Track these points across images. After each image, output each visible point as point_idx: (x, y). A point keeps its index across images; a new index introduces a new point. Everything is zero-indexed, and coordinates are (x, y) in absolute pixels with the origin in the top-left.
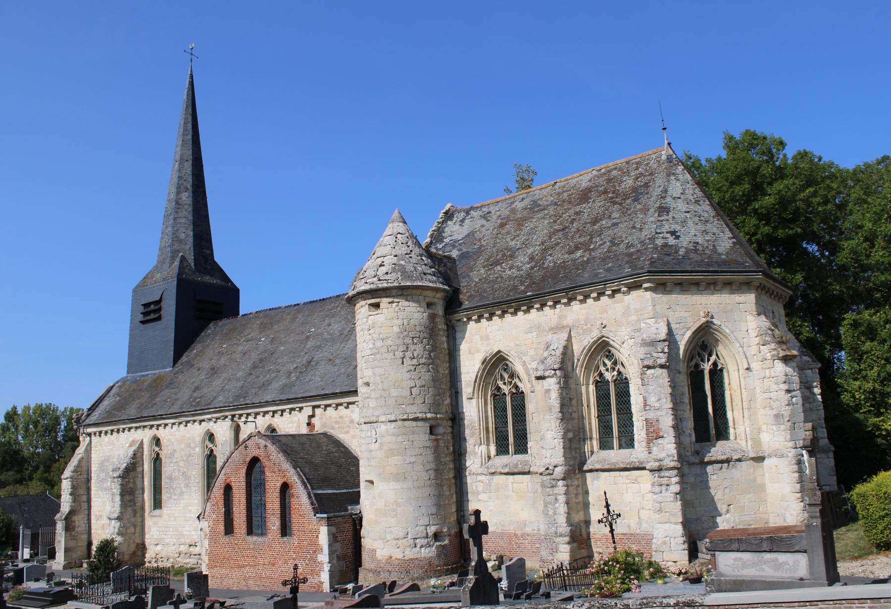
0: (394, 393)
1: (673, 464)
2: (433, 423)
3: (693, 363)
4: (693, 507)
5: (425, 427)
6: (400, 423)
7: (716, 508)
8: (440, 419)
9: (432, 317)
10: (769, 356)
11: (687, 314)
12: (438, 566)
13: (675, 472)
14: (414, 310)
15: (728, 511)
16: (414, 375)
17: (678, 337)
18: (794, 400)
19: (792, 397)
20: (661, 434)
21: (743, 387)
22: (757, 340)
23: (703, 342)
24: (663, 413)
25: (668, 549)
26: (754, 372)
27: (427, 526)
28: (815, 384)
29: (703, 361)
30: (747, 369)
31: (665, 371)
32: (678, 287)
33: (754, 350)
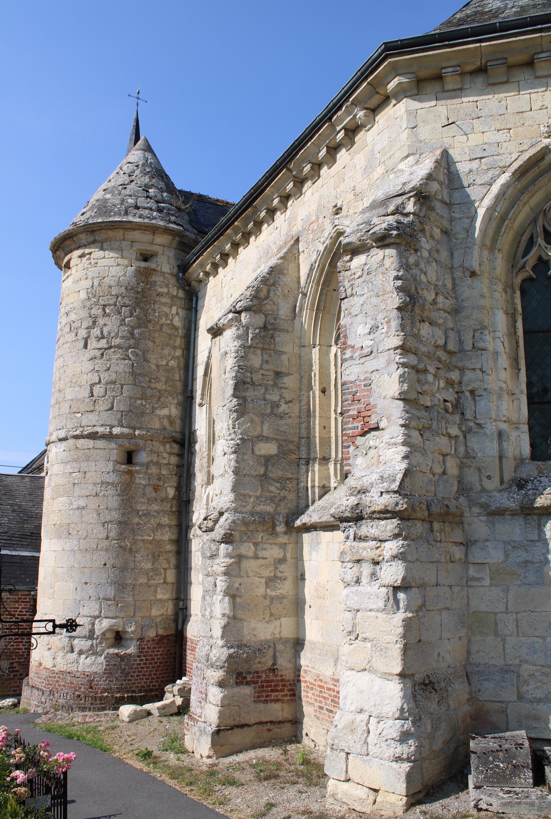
0: (70, 394)
1: (387, 501)
2: (127, 444)
5: (112, 450)
6: (71, 442)
8: (141, 437)
9: (144, 275)
11: (501, 137)
12: (105, 690)
14: (111, 262)
16: (100, 364)
17: (474, 193)
20: (373, 421)
24: (379, 362)
25: (357, 748)
27: (96, 617)
32: (480, 80)
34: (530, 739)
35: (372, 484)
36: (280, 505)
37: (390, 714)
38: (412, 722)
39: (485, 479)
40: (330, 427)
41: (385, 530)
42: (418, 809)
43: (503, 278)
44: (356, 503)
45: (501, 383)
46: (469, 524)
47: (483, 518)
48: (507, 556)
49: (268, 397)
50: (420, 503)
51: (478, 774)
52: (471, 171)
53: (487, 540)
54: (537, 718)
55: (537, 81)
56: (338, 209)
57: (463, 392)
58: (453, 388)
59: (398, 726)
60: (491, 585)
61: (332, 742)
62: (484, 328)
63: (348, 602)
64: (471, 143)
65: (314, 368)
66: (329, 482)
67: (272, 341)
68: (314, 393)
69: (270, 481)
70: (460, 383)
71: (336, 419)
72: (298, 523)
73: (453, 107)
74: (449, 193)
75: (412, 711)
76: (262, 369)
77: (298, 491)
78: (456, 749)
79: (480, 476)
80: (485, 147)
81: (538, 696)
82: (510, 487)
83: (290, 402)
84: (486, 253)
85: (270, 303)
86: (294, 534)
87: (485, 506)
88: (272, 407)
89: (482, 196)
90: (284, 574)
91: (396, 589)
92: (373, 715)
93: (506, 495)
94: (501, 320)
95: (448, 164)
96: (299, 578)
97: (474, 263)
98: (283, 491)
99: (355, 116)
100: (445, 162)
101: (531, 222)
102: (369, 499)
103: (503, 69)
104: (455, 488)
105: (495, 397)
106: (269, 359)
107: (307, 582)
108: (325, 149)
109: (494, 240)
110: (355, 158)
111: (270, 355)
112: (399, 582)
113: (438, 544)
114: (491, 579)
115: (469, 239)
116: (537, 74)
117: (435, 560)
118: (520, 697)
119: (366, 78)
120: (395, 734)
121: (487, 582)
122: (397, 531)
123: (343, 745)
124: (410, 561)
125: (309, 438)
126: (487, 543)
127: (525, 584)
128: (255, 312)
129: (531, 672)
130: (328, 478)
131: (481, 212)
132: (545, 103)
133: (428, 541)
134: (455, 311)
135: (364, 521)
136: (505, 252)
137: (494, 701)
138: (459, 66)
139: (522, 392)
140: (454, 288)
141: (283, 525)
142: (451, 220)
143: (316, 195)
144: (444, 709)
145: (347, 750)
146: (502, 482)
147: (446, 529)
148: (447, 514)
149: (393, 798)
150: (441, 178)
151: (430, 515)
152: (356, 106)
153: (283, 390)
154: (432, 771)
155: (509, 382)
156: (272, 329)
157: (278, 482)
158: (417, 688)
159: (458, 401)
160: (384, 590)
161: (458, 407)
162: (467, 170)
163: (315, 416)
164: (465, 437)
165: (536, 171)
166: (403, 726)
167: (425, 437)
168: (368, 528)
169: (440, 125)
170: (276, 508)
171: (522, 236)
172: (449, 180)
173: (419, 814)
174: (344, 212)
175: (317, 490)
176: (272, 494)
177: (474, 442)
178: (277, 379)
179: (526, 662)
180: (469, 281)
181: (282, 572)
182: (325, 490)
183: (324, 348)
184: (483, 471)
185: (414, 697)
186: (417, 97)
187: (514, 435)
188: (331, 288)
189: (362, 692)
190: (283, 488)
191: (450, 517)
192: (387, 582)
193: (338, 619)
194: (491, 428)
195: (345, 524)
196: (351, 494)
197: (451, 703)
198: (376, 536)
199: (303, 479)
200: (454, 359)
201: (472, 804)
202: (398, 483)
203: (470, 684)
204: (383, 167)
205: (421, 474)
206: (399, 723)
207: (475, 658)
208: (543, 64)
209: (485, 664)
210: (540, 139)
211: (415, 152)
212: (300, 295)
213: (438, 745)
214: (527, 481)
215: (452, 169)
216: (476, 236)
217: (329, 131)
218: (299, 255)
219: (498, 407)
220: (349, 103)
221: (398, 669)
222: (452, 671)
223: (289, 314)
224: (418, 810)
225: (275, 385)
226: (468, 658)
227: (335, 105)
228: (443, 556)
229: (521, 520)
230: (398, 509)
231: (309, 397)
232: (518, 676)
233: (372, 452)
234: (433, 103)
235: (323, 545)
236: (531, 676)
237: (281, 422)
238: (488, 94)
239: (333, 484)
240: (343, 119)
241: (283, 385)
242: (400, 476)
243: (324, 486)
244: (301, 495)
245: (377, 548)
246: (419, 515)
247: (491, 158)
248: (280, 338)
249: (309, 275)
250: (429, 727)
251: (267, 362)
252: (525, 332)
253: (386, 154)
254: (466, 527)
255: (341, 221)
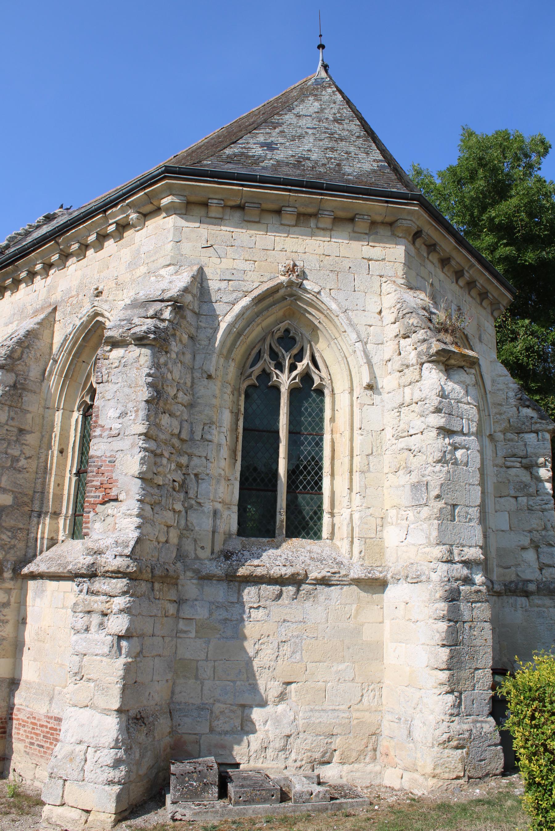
3: (257, 369)
4: (197, 678)
7: (254, 688)
10: (412, 357)
11: (247, 266)
13: (121, 584)
15: (282, 697)
17: (219, 308)
18: (459, 454)
19: (456, 449)
20: (113, 493)
21: (356, 425)
22: (395, 329)
23: (287, 331)
24: (124, 444)
25: (75, 775)
26: (385, 396)
28: (541, 460)
29: (280, 367)
30: (370, 387)
31: (146, 351)
32: (237, 215)
33: (389, 349)
34: (219, 765)
35: (107, 547)
36: (9, 553)
37: (107, 744)
38: (125, 750)
39: (199, 549)
40: (63, 485)
41: (115, 588)
42: (124, 824)
43: (232, 383)
44: (92, 562)
45: (221, 470)
46: (183, 586)
47: (195, 581)
48: (211, 614)
49: (9, 451)
50: (147, 566)
51: (176, 792)
52: (219, 289)
53: (196, 600)
54: (223, 747)
55: (282, 227)
56: (99, 293)
57: (189, 474)
58: (181, 470)
59: (112, 754)
60: (196, 637)
61: (51, 771)
62: (212, 423)
63: (77, 648)
64: (223, 266)
65: (55, 430)
66: (58, 535)
67: (20, 400)
68: (52, 452)
69: (3, 530)
70: (187, 466)
71: (70, 478)
72: (25, 570)
73: (213, 232)
74: (199, 305)
75: (126, 741)
76: (7, 425)
77: (27, 541)
78: (157, 774)
79: (195, 545)
80: (234, 271)
81: (226, 729)
82: (219, 557)
83: (30, 458)
84: (222, 360)
85: (23, 364)
86: (20, 581)
87: (197, 572)
88: (12, 461)
89: (225, 312)
90: (7, 617)
91: (120, 638)
92: (91, 745)
93: (215, 563)
94: (227, 417)
95: (202, 279)
96: (21, 621)
97: (212, 368)
98: (14, 540)
99: (128, 216)
100: (200, 278)
101: (261, 340)
102: (104, 560)
103: (257, 212)
104: (174, 555)
105: (214, 481)
106: (15, 416)
107: (28, 626)
108: (95, 235)
109: (230, 351)
110: (122, 251)
111: (16, 413)
112: (124, 632)
113: (157, 601)
114: (196, 632)
115: (210, 347)
116: (283, 222)
117: (153, 614)
118: (212, 730)
119: (144, 188)
120: (110, 762)
121: (193, 635)
122: (125, 589)
123: (62, 773)
124: (133, 615)
125: (43, 493)
126: (196, 603)
127: (223, 638)
128: (8, 371)
129: (222, 710)
130: (57, 531)
131: (223, 326)
132: (285, 247)
133: (149, 599)
134: (191, 406)
135: (97, 578)
136: (237, 361)
137: (190, 734)
138: (223, 200)
139: (236, 479)
140: (192, 386)
141: (11, 572)
142: (198, 328)
143: (79, 273)
144: (150, 740)
145: (64, 778)
146: (212, 553)
147: (165, 589)
148: (167, 576)
149: (103, 817)
150: (195, 291)
151: (153, 576)
152: (130, 208)
153: (24, 446)
154: (137, 792)
155: (227, 469)
156: (21, 389)
157: (10, 531)
158: (130, 722)
159: (184, 481)
160: (110, 638)
161: (183, 487)
162: (217, 288)
163: (51, 474)
164: (186, 512)
165: (271, 300)
166: (117, 754)
167: (155, 511)
168: (100, 585)
169: (200, 245)
170: (6, 555)
171: (252, 349)
172: (201, 293)
173: (125, 828)
174: (104, 297)
175: (45, 542)
176: (3, 542)
177: (193, 517)
178: (20, 436)
179: (219, 701)
180: (205, 382)
181: (5, 616)
182: (53, 542)
183: (67, 412)
184: (198, 542)
185: (128, 729)
186: (185, 216)
187: (226, 513)
188: (81, 360)
189: (82, 725)
190: (14, 537)
191: (169, 579)
192: (113, 632)
193: (56, 662)
194: (208, 507)
195: (80, 579)
196: (88, 554)
197: (156, 735)
198: (107, 592)
199: (33, 530)
200: (185, 446)
201: (170, 816)
202: (130, 549)
203: (172, 720)
204: (146, 268)
205: (149, 542)
206: (113, 751)
207: (178, 698)
208: (288, 216)
209: (185, 703)
210: (277, 275)
211: (175, 263)
212: (51, 361)
213: (143, 771)
214: (232, 554)
215: (204, 284)
216: (216, 345)
217: (101, 221)
218: (55, 323)
219: (216, 490)
220: (125, 204)
221: (117, 706)
222: (159, 708)
223: (38, 377)
224: (124, 825)
225: (17, 440)
226: (172, 698)
227: (111, 201)
228: (160, 612)
229: (225, 585)
230: (128, 570)
231: (47, 455)
232: (212, 713)
233: (109, 520)
234: (197, 225)
235: (48, 593)
236: (222, 712)
237: (18, 476)
238: (242, 228)
239: (61, 537)
240: (117, 214)
241: (25, 442)
242: (132, 543)
243: (52, 539)
244: (30, 544)
245: (107, 602)
246: (145, 576)
247: (237, 282)
248: (28, 397)
249: (62, 345)
250: (137, 755)
251: (13, 419)
252: (244, 429)
253: (150, 257)
254: (180, 587)
255: (100, 304)
